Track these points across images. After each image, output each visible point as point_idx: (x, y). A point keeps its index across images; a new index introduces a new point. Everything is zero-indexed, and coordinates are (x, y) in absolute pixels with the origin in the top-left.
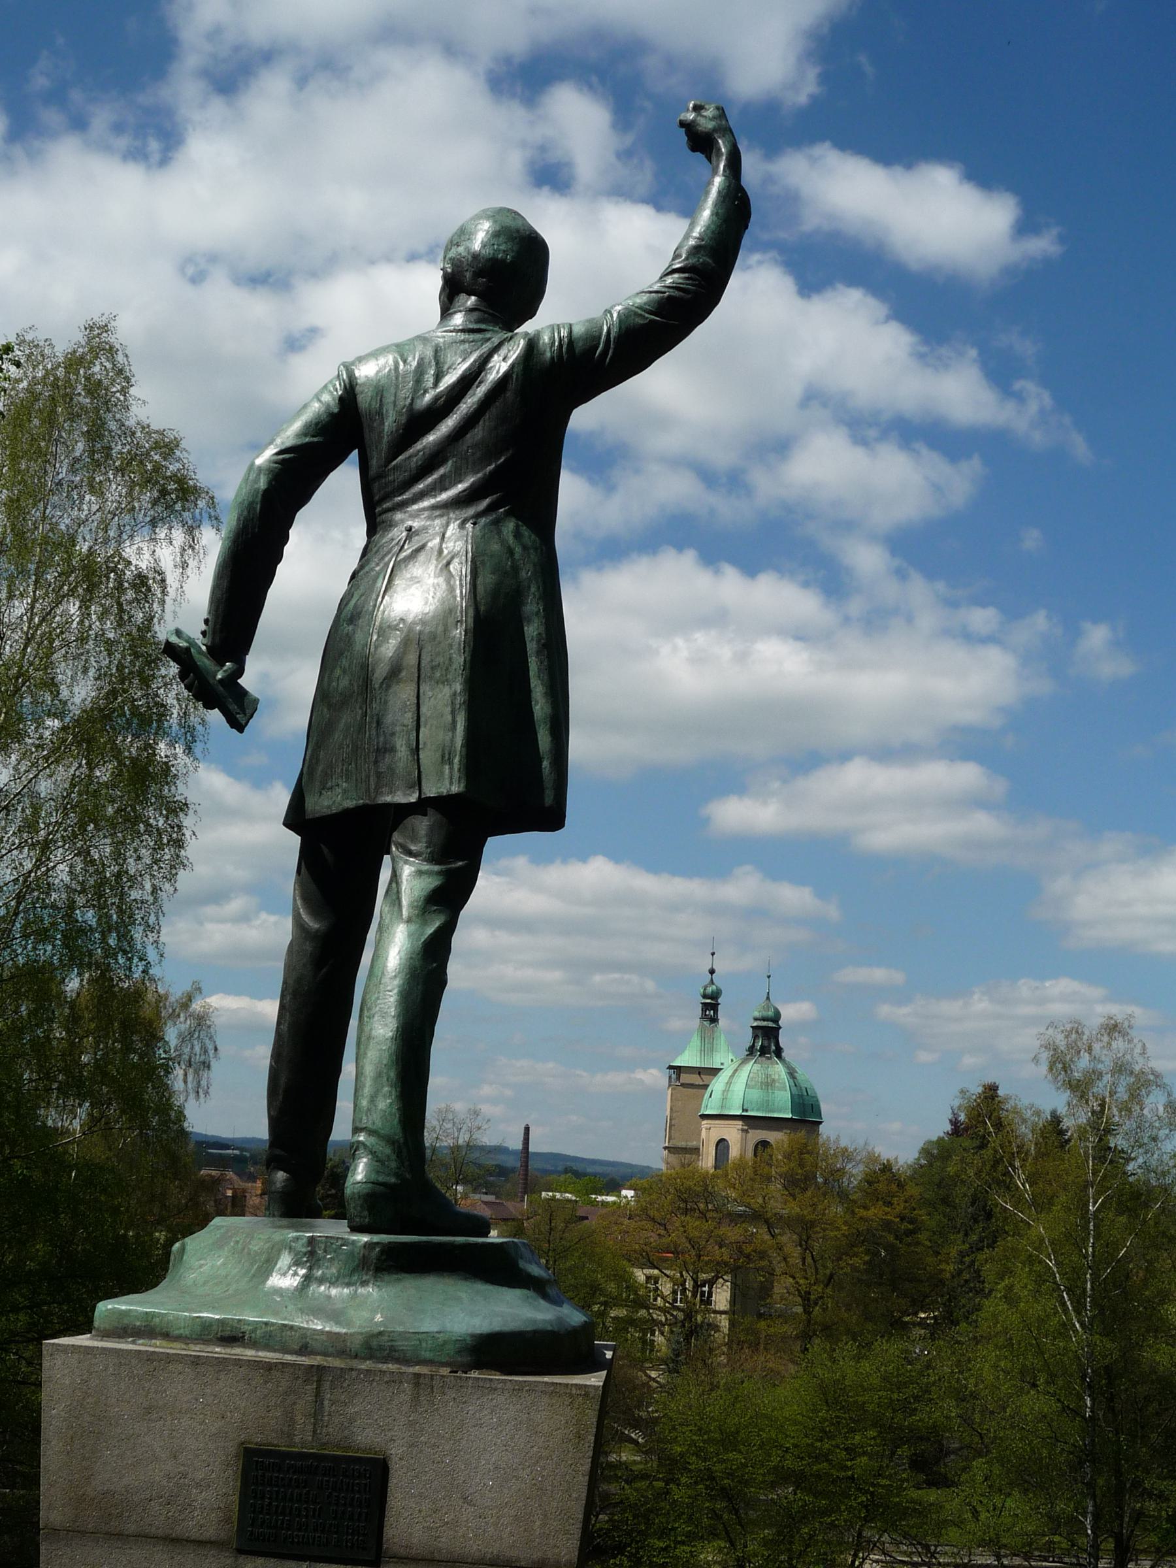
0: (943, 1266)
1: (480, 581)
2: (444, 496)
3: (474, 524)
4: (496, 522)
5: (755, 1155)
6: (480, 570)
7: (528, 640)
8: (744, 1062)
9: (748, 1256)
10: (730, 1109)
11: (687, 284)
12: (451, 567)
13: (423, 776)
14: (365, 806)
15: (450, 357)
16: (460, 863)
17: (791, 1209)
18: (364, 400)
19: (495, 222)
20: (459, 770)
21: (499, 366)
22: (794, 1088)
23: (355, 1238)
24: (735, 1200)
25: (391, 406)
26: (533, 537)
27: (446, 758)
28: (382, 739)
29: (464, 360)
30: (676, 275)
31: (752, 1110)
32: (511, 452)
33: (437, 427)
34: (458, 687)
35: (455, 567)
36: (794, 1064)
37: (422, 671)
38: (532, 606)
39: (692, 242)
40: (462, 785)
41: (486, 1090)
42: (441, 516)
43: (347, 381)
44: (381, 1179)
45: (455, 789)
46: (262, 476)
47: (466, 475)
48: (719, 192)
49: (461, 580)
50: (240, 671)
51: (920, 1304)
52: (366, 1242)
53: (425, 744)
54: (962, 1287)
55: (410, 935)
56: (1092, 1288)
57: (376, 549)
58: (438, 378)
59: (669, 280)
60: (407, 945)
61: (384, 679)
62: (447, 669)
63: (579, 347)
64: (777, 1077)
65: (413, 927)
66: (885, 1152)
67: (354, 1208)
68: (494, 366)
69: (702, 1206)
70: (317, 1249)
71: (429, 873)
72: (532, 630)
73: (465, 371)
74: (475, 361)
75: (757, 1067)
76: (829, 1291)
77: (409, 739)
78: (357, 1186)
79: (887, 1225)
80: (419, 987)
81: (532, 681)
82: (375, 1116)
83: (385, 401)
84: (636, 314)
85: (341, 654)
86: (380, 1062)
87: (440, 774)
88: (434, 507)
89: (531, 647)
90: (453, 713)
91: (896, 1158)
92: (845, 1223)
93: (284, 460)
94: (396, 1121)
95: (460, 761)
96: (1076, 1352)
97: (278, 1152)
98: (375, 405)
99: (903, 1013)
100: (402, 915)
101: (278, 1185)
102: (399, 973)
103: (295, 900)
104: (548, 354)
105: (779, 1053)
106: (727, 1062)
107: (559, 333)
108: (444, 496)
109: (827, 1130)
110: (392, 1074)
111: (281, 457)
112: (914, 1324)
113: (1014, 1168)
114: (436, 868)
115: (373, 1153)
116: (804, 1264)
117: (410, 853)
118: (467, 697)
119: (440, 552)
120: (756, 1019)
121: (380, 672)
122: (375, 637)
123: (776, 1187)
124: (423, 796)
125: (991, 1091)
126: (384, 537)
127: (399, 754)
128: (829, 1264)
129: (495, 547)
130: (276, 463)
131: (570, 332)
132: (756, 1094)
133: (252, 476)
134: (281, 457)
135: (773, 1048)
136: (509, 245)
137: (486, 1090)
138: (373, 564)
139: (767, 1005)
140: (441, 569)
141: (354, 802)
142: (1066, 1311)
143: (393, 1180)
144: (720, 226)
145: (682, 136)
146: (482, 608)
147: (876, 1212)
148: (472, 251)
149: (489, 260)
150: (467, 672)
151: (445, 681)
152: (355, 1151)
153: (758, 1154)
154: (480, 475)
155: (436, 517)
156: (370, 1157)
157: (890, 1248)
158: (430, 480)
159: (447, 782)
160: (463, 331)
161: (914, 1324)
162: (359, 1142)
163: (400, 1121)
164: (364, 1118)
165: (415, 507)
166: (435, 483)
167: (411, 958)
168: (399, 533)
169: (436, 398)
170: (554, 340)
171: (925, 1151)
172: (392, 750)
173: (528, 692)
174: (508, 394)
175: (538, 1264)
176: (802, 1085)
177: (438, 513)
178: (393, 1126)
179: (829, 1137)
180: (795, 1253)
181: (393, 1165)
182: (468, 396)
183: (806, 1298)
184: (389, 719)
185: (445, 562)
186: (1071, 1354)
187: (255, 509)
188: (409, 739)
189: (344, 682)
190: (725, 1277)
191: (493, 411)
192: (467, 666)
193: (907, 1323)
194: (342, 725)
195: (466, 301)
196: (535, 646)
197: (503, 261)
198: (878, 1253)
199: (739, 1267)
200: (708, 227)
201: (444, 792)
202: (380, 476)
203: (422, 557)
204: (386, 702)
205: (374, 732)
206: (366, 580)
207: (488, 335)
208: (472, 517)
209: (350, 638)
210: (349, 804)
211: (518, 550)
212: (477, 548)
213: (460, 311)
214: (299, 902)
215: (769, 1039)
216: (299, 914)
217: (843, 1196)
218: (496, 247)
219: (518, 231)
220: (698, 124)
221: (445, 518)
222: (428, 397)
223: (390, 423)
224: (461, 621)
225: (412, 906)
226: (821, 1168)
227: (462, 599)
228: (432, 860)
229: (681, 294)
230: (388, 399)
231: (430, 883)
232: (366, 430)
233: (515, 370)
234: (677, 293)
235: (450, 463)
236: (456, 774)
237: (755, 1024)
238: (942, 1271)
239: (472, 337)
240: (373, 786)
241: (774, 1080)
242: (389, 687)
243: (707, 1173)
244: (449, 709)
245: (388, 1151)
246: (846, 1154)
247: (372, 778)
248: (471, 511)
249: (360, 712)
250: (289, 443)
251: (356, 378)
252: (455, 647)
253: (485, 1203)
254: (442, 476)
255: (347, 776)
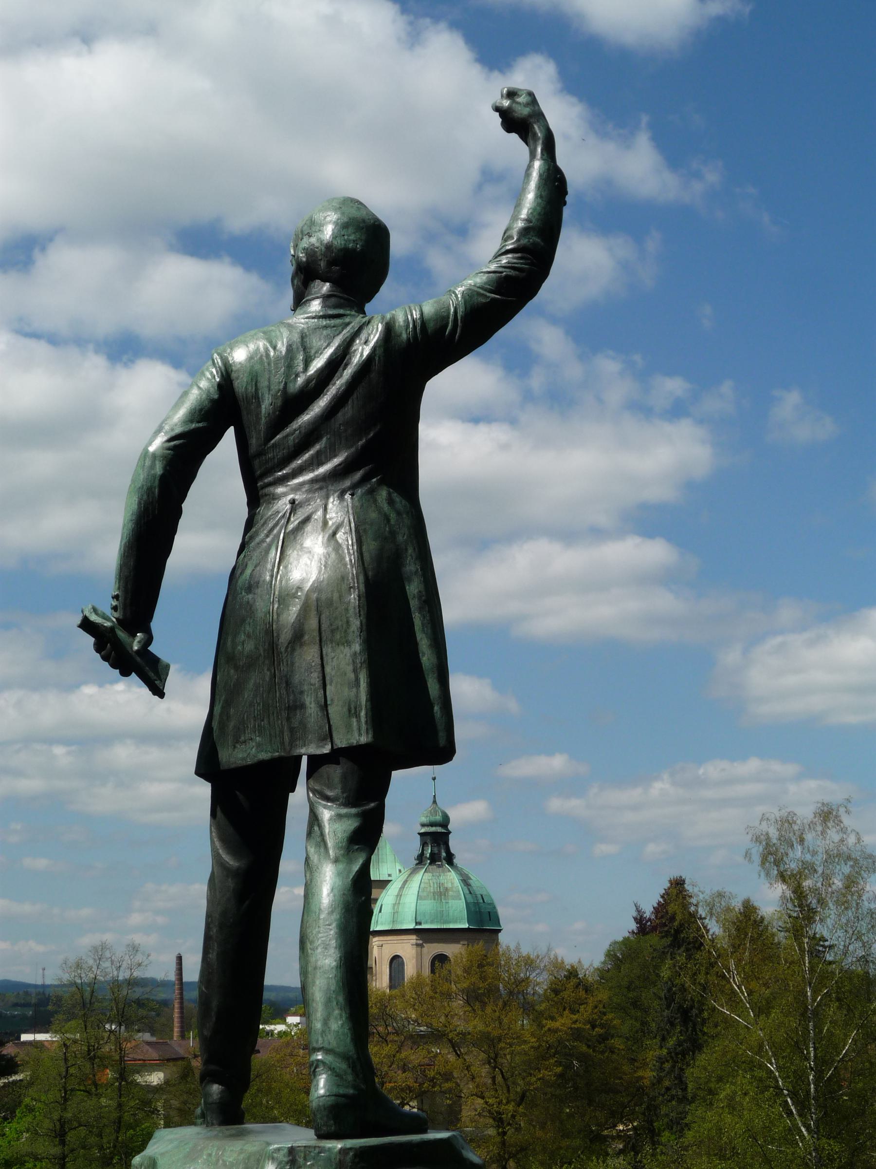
0: (640, 1073)
1: (364, 548)
2: (322, 470)
3: (352, 495)
4: (371, 492)
5: (433, 971)
6: (364, 538)
7: (410, 597)
8: (414, 871)
9: (432, 1080)
10: (402, 923)
11: (522, 264)
12: (338, 536)
13: (333, 728)
14: (280, 759)
15: (315, 342)
16: (372, 805)
17: (476, 1025)
18: (240, 384)
19: (343, 214)
20: (366, 722)
21: (362, 351)
22: (469, 897)
23: (330, 1145)
24: (416, 1021)
25: (266, 390)
26: (404, 502)
27: (352, 711)
28: (291, 697)
29: (328, 345)
30: (510, 256)
31: (426, 923)
32: (379, 427)
33: (310, 407)
34: (357, 647)
35: (340, 536)
36: (467, 870)
37: (323, 634)
38: (411, 566)
39: (520, 224)
40: (370, 736)
41: (136, 919)
42: (321, 488)
43: (223, 369)
44: (341, 1092)
45: (364, 740)
46: (157, 462)
47: (340, 451)
48: (541, 176)
49: (348, 549)
50: (149, 640)
51: (617, 1116)
52: (341, 1149)
53: (332, 700)
54: (663, 1095)
55: (339, 874)
56: (816, 1089)
57: (262, 521)
58: (307, 363)
59: (504, 260)
60: (339, 882)
61: (289, 644)
62: (346, 631)
63: (431, 327)
64: (450, 885)
65: (341, 866)
66: (569, 956)
67: (321, 1119)
68: (358, 349)
69: (381, 1029)
70: (297, 1157)
71: (347, 816)
72: (413, 588)
73: (331, 355)
74: (339, 346)
75: (428, 876)
76: (521, 1109)
77: (317, 697)
78: (321, 1099)
79: (577, 1034)
80: (354, 920)
81: (417, 635)
82: (329, 1037)
83: (260, 385)
84: (479, 294)
85: (243, 621)
86: (328, 989)
87: (349, 727)
88: (313, 481)
89: (414, 604)
90: (355, 671)
91: (580, 962)
92: (533, 1035)
93: (175, 446)
94: (349, 1040)
95: (366, 714)
96: (805, 1157)
97: (212, 1067)
98: (251, 389)
99: (574, 805)
100: (329, 855)
101: (215, 1097)
102: (335, 908)
103: (212, 842)
104: (404, 336)
105: (450, 859)
106: (395, 874)
107: (412, 315)
108: (322, 470)
109: (505, 939)
110: (341, 999)
111: (172, 443)
112: (613, 1138)
113: (729, 971)
114: (353, 811)
115: (331, 1069)
116: (494, 1083)
117: (328, 799)
118: (366, 656)
119: (325, 523)
120: (423, 825)
121: (285, 636)
122: (276, 606)
123: (458, 1004)
124: (335, 747)
125: (678, 884)
126: (269, 509)
127: (309, 711)
128: (521, 1082)
129: (373, 515)
130: (169, 449)
131: (422, 314)
132: (428, 905)
133: (148, 463)
134: (172, 443)
135: (444, 854)
136: (358, 235)
137: (136, 919)
138: (262, 536)
139: (434, 809)
140: (329, 540)
141: (270, 754)
142: (790, 1113)
143: (351, 1091)
144: (544, 208)
145: (497, 119)
146: (370, 574)
147: (563, 1022)
148: (325, 242)
149: (341, 250)
150: (364, 634)
151: (348, 643)
152: (316, 1068)
153: (436, 971)
154: (353, 450)
155: (316, 490)
156: (330, 1072)
157: (583, 1058)
158: (307, 456)
159: (356, 734)
160: (324, 317)
161: (613, 1138)
162: (318, 1060)
163: (352, 1039)
164: (320, 1039)
165: (296, 481)
166: (312, 458)
167: (344, 894)
168: (283, 505)
169: (308, 381)
170: (408, 323)
171: (610, 955)
172: (303, 706)
173: (416, 644)
174: (373, 375)
175: (476, 1155)
176: (478, 893)
177: (317, 486)
178: (347, 1045)
179: (508, 947)
180: (483, 1072)
181: (350, 1078)
182: (335, 378)
183: (499, 1120)
184: (296, 679)
185: (331, 531)
186: (799, 1161)
187: (153, 493)
188: (317, 697)
189: (249, 646)
190: (411, 1103)
191: (360, 391)
192: (364, 628)
193: (607, 1136)
194: (251, 685)
195: (322, 288)
196: (417, 603)
197: (354, 250)
198: (569, 1066)
199: (425, 1092)
200: (534, 209)
201: (355, 742)
202: (260, 454)
203: (309, 528)
204: (293, 664)
205: (284, 692)
206: (258, 551)
207: (347, 320)
208: (349, 488)
209: (251, 606)
210: (264, 756)
211: (393, 516)
212: (358, 518)
213: (318, 298)
214: (218, 844)
215: (439, 845)
216: (218, 854)
217: (528, 1008)
218: (346, 237)
219: (364, 221)
220: (514, 111)
221: (325, 490)
222: (300, 380)
223: (267, 405)
224: (353, 587)
225: (336, 847)
226: (504, 979)
227: (352, 567)
228: (347, 804)
229: (517, 273)
230: (263, 383)
231: (350, 825)
232: (244, 413)
233: (377, 352)
234: (512, 273)
235: (324, 439)
236: (364, 727)
237: (423, 830)
238: (642, 1078)
239: (333, 322)
240: (287, 739)
241: (447, 889)
242: (293, 650)
243: (384, 993)
244: (351, 668)
245: (344, 1066)
246: (529, 963)
247: (286, 734)
248: (347, 483)
249: (268, 673)
250: (178, 430)
251: (231, 365)
252: (351, 611)
253: (149, 1043)
254: (318, 451)
255: (261, 731)
